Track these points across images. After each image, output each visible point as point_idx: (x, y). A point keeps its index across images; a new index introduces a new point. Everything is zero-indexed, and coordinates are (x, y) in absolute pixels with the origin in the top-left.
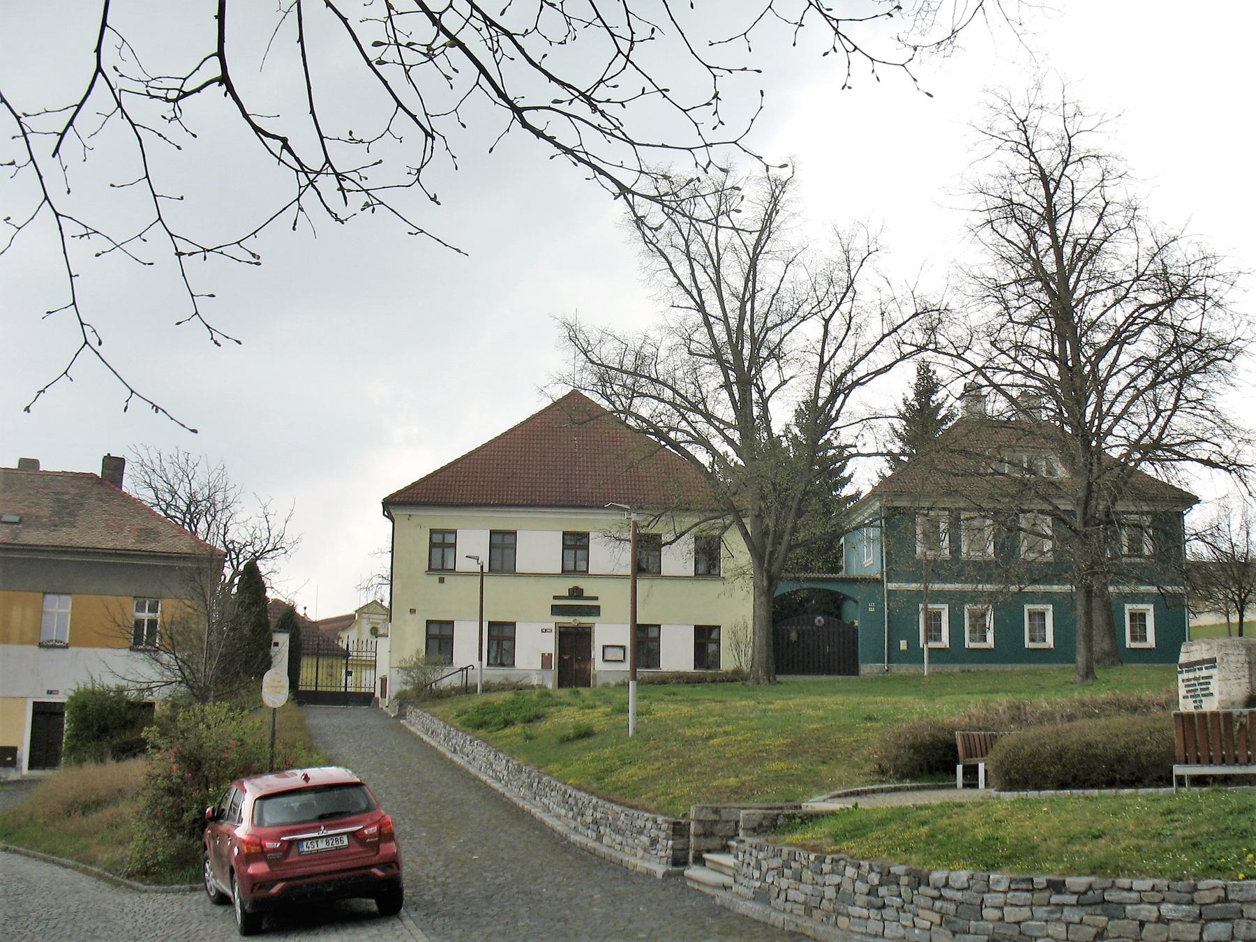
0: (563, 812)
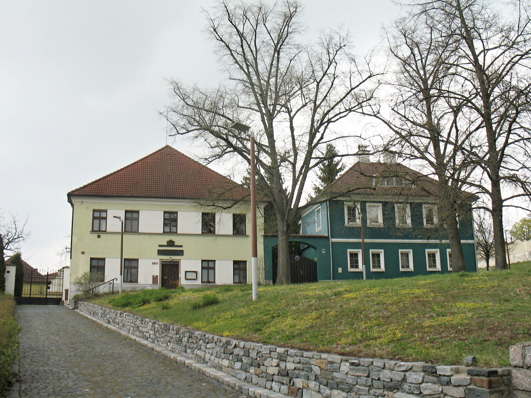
0: (226, 363)
